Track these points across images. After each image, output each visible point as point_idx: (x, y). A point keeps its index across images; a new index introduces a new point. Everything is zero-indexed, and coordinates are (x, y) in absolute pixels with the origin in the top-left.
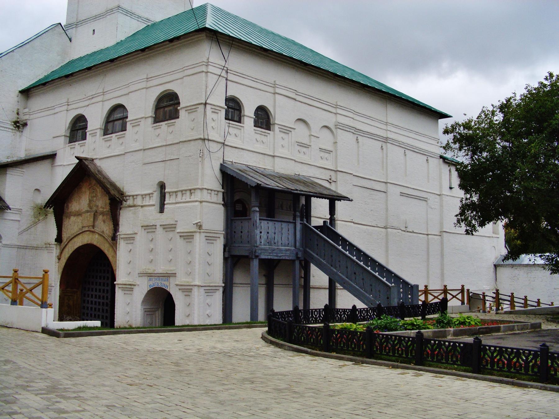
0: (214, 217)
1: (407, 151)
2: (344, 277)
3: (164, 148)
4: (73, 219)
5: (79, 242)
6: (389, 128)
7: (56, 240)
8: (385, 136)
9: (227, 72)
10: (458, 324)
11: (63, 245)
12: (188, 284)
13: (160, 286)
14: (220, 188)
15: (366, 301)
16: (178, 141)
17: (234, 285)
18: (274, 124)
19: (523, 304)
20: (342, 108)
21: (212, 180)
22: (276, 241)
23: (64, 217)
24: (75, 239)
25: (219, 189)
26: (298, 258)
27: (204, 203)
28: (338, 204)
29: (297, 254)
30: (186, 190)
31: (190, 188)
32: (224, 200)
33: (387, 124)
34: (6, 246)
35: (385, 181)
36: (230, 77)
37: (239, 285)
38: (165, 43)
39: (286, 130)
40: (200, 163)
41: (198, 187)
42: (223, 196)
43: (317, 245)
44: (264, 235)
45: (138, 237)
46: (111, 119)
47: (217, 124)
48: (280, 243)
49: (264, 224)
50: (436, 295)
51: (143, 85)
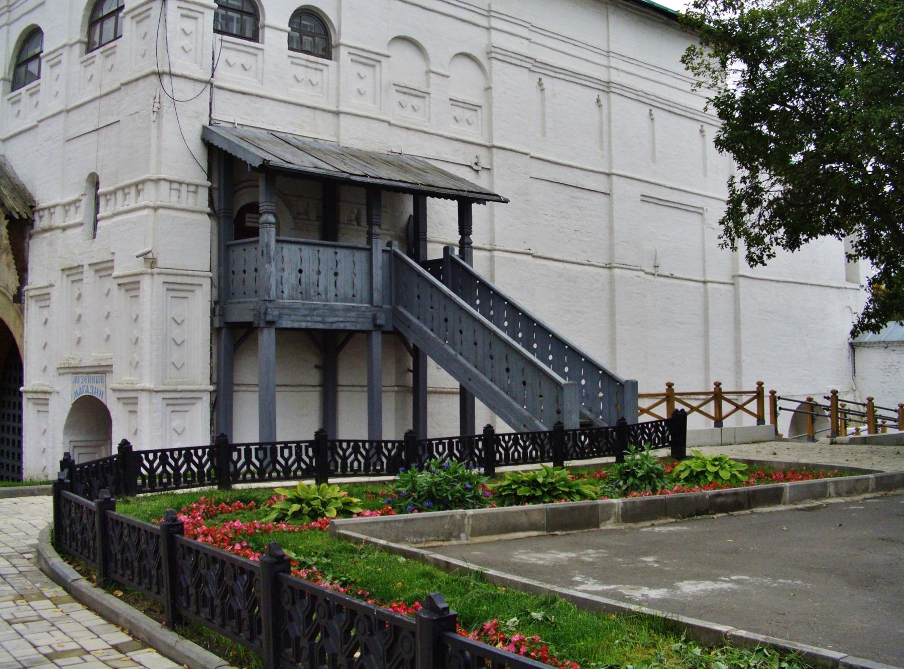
0: (191, 241)
1: (654, 111)
2: (469, 365)
3: (96, 103)
6: (614, 62)
8: (604, 78)
10: (686, 479)
12: (130, 387)
13: (90, 392)
14: (201, 178)
15: (513, 420)
16: (117, 85)
17: (339, 388)
18: (338, 45)
19: (895, 420)
20: (501, 17)
21: (184, 162)
22: (321, 288)
25: (198, 181)
26: (378, 327)
27: (160, 211)
28: (477, 209)
29: (374, 318)
30: (129, 186)
32: (211, 203)
33: (608, 54)
35: (607, 171)
37: (346, 388)
39: (369, 59)
40: (154, 126)
41: (147, 176)
42: (210, 195)
43: (419, 297)
44: (290, 277)
45: (55, 293)
46: (25, 58)
48: (331, 295)
49: (290, 252)
50: (695, 404)
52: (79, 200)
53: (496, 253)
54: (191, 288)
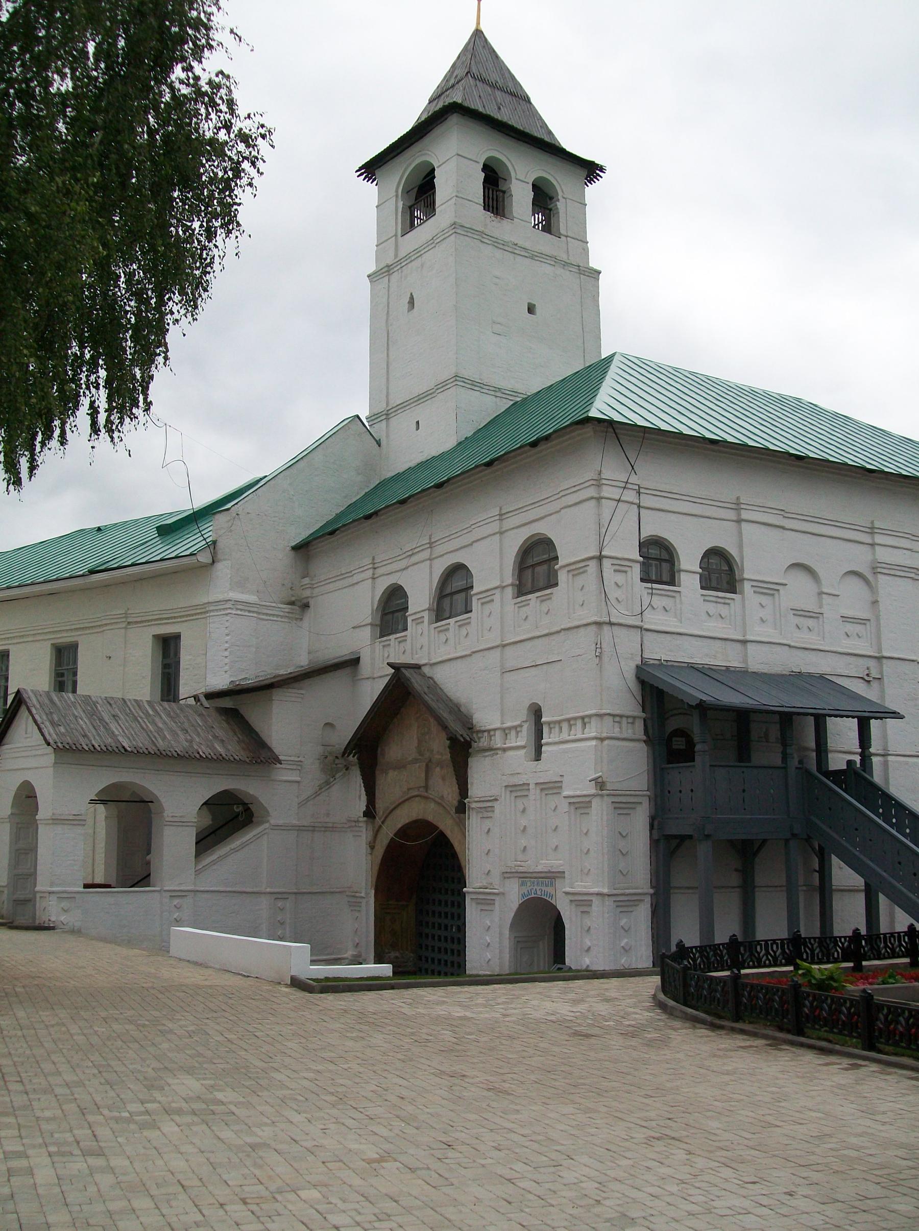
0: (632, 766)
4: (392, 774)
5: (403, 817)
7: (366, 814)
9: (639, 493)
11: (378, 821)
14: (638, 712)
16: (559, 629)
18: (743, 580)
21: (616, 691)
23: (377, 772)
24: (398, 812)
25: (636, 714)
30: (575, 719)
31: (581, 714)
34: (277, 827)
36: (646, 501)
38: (523, 450)
42: (645, 725)
46: (448, 591)
47: (629, 587)
51: (495, 527)
52: (521, 726)
53: (890, 758)
54: (632, 806)
